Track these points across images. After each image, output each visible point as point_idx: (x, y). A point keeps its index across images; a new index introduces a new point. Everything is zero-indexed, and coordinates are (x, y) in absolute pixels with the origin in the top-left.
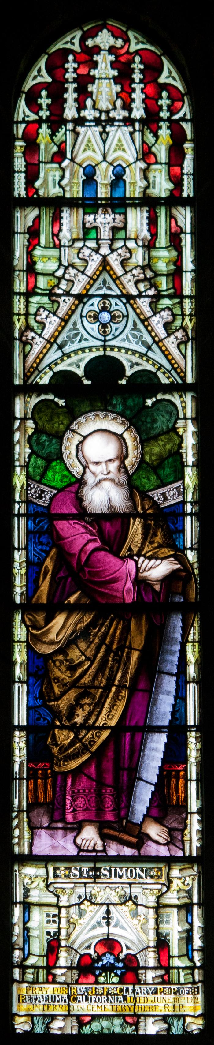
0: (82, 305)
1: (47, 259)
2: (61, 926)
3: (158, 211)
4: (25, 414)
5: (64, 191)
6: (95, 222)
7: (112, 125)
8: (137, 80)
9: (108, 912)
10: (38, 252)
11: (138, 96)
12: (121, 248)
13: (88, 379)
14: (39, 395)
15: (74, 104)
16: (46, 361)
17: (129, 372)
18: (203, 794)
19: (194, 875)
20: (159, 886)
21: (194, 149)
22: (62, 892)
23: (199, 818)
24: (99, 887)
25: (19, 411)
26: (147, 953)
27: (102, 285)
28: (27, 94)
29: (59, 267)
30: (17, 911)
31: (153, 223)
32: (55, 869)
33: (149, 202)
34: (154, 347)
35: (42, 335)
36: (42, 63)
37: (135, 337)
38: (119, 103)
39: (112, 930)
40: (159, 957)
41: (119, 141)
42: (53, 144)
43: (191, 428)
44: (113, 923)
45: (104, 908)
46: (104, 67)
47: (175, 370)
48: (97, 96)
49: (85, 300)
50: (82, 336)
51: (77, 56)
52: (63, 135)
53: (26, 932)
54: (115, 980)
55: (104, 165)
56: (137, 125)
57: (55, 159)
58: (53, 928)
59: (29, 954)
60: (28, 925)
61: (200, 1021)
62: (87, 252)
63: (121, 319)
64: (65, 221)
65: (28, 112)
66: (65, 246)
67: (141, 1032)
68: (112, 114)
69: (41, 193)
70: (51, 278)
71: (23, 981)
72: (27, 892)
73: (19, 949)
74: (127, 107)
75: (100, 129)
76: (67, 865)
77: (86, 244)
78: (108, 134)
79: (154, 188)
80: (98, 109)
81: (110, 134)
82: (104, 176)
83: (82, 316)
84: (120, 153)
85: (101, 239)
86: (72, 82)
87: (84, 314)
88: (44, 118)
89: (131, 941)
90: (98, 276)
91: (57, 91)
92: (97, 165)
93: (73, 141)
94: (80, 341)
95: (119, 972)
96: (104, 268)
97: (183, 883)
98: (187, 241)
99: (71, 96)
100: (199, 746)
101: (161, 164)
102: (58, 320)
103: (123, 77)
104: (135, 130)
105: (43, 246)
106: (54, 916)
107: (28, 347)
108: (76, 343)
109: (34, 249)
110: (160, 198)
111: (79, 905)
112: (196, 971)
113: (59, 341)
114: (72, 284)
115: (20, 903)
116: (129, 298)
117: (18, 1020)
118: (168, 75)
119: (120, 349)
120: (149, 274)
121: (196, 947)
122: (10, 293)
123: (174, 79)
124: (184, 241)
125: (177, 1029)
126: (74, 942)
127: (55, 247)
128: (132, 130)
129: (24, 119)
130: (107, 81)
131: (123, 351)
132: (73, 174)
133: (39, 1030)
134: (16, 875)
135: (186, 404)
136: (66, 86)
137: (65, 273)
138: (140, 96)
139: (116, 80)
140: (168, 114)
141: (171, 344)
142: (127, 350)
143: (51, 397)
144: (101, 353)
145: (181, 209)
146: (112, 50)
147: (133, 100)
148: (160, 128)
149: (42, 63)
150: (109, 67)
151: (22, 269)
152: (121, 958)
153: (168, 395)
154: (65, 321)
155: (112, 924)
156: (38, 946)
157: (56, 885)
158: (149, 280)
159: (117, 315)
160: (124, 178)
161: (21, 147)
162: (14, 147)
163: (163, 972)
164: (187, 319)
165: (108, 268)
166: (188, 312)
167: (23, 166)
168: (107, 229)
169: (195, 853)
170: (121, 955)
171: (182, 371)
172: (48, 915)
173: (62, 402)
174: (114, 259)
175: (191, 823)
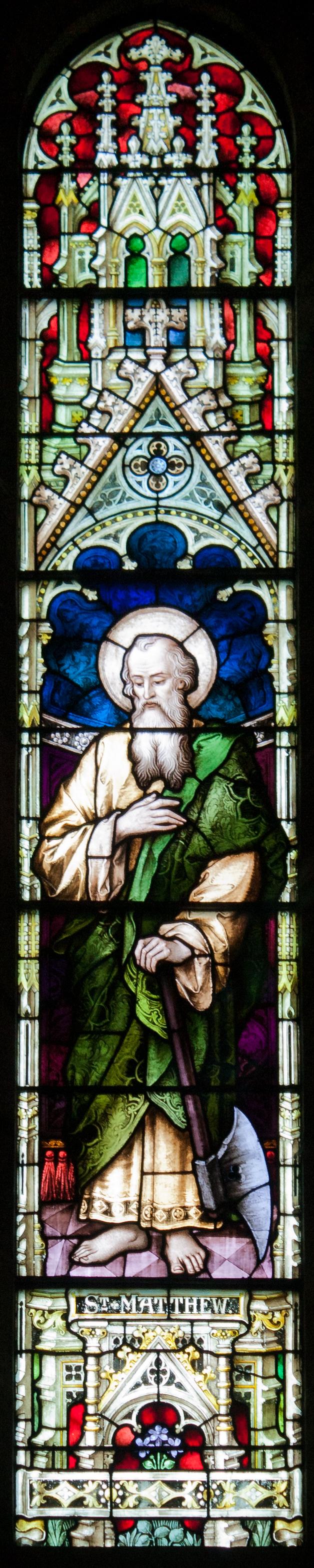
0: (123, 450)
1: (71, 380)
4: (38, 614)
5: (98, 277)
6: (142, 319)
7: (168, 176)
8: (206, 110)
9: (158, 1362)
10: (55, 370)
11: (207, 132)
12: (182, 360)
13: (132, 557)
14: (58, 584)
15: (111, 144)
16: (69, 534)
17: (193, 549)
19: (287, 1309)
20: (236, 1326)
21: (292, 211)
22: (91, 1333)
23: (297, 1224)
24: (145, 1326)
25: (26, 612)
26: (217, 1423)
27: (154, 419)
28: (40, 128)
29: (89, 393)
30: (22, 1362)
31: (228, 328)
32: (80, 1301)
33: (223, 292)
34: (232, 511)
35: (64, 495)
36: (62, 83)
37: (203, 494)
38: (179, 143)
39: (164, 1389)
41: (180, 198)
42: (81, 205)
44: (165, 1378)
45: (153, 1357)
46: (157, 88)
47: (263, 546)
48: (145, 133)
49: (129, 441)
50: (124, 493)
51: (115, 73)
53: (36, 1394)
54: (168, 1464)
55: (158, 234)
56: (205, 177)
57: (84, 228)
58: (75, 1387)
59: (41, 1427)
61: (297, 1527)
62: (129, 367)
63: (182, 468)
64: (96, 320)
65: (42, 157)
66: (96, 359)
67: (207, 1544)
68: (168, 159)
69: (63, 279)
70: (78, 408)
71: (32, 1468)
72: (37, 1334)
73: (26, 1420)
74: (191, 148)
75: (150, 181)
76: (115, 1293)
77: (129, 355)
78: (161, 188)
79: (232, 269)
80: (147, 153)
81: (166, 189)
82: (156, 251)
85: (150, 347)
88: (66, 164)
89: (194, 1408)
90: (147, 405)
91: (87, 114)
92: (145, 234)
93: (111, 201)
95: (174, 1453)
96: (158, 392)
97: (271, 1321)
99: (106, 133)
100: (296, 1114)
101: (243, 233)
102: (87, 472)
103: (185, 109)
104: (202, 184)
106: (78, 1368)
107: (42, 513)
108: (114, 505)
109: (51, 364)
110: (241, 289)
111: (115, 1351)
112: (290, 1453)
113: (89, 503)
115: (27, 1351)
116: (194, 438)
117: (22, 1526)
118: (254, 99)
119: (179, 510)
120: (225, 401)
121: (289, 1415)
122: (14, 435)
124: (276, 351)
125: (261, 1539)
126: (106, 1409)
127: (82, 360)
129: (36, 166)
130: (160, 111)
131: (184, 514)
132: (111, 251)
133: (55, 1541)
134: (21, 1309)
135: (279, 602)
136: (99, 118)
137: (98, 401)
138: (209, 133)
139: (174, 109)
140: (252, 159)
141: (256, 507)
142: (190, 512)
143: (77, 587)
144: (151, 518)
145: (272, 304)
146: (167, 65)
147: (199, 139)
148: (240, 180)
149: (62, 83)
150: (163, 90)
151: (33, 395)
152: (177, 1432)
153: (251, 584)
155: (165, 1381)
156: (54, 1415)
157: (80, 1323)
158: (225, 410)
159: (176, 462)
160: (187, 253)
161: (32, 210)
162: (22, 211)
163: (242, 1452)
164: (281, 468)
165: (163, 392)
166: (280, 457)
167: (36, 241)
168: (160, 332)
169: (289, 1275)
170: (177, 1426)
171: (272, 549)
172: (69, 1368)
173: (92, 595)
174: (171, 377)
175: (284, 1229)
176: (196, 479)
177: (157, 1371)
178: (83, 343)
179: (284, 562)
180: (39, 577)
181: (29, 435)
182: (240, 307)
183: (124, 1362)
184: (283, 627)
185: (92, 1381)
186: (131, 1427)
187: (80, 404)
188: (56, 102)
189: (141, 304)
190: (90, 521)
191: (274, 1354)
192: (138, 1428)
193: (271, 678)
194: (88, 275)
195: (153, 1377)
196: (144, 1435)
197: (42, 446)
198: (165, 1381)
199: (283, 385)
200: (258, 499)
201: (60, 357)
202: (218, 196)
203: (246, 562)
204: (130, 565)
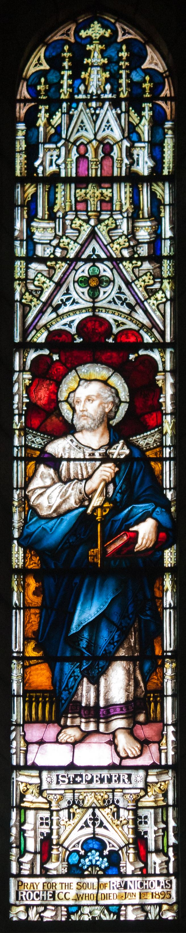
2: (52, 827)
3: (140, 186)
9: (94, 814)
13: (79, 337)
14: (36, 351)
17: (115, 330)
18: (178, 710)
20: (138, 791)
37: (119, 298)
38: (108, 87)
40: (161, 273)
43: (170, 380)
44: (98, 823)
45: (91, 811)
52: (59, 119)
58: (45, 830)
59: (26, 851)
60: (24, 828)
64: (59, 196)
72: (22, 796)
79: (138, 164)
83: (74, 282)
84: (108, 132)
86: (67, 70)
87: (76, 279)
94: (72, 304)
98: (166, 215)
101: (144, 142)
103: (111, 66)
105: (41, 218)
106: (47, 819)
109: (33, 221)
111: (69, 808)
114: (66, 252)
123: (156, 64)
128: (119, 112)
134: (13, 782)
135: (164, 359)
143: (46, 352)
152: (104, 854)
154: (59, 285)
155: (97, 825)
162: (15, 131)
164: (166, 282)
166: (165, 274)
176: (116, 287)
177: (94, 818)
178: (51, 204)
179: (168, 339)
180: (26, 346)
181: (20, 258)
182: (142, 187)
183: (74, 814)
184: (169, 375)
185: (55, 827)
186: (78, 852)
187: (49, 244)
188: (37, 63)
189: (84, 186)
190: (54, 315)
191: (162, 807)
192: (82, 852)
193: (161, 405)
194: (54, 168)
195: (91, 822)
196: (85, 856)
197: (27, 268)
198: (97, 825)
199: (167, 232)
200: (152, 301)
201: (38, 217)
202: (131, 120)
203: (147, 339)
204: (79, 340)
